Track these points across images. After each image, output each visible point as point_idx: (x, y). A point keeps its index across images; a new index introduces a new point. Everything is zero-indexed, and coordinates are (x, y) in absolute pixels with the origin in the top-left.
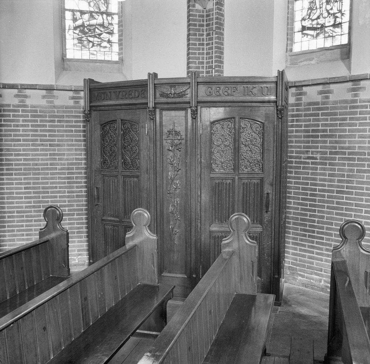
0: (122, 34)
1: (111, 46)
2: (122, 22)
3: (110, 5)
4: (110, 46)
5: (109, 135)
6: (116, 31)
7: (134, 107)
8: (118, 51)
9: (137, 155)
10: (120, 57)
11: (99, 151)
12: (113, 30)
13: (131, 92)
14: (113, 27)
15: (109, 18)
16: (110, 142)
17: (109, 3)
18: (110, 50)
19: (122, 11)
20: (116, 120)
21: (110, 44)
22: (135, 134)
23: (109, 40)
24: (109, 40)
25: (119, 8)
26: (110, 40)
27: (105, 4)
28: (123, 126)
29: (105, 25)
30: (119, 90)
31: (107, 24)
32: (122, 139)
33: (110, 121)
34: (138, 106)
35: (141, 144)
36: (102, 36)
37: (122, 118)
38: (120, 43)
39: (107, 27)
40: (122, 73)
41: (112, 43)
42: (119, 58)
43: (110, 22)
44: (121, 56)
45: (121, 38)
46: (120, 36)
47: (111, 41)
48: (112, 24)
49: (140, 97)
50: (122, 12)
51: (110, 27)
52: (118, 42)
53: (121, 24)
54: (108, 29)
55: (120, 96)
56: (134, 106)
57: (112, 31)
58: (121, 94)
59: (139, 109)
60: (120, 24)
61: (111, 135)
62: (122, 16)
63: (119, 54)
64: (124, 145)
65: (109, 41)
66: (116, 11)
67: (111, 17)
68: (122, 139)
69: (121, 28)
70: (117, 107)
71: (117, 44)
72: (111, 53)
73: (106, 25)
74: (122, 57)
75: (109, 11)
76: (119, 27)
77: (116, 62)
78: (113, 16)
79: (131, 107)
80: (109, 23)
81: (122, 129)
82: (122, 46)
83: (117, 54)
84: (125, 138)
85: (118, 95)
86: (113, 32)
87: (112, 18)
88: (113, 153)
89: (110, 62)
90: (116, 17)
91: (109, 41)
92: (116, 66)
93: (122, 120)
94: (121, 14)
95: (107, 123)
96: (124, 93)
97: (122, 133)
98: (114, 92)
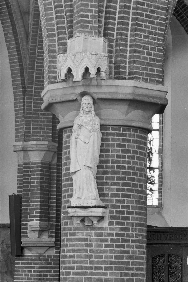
0: (162, 184)
1: (153, 193)
2: (162, 175)
3: (152, 162)
4: (151, 193)
5: (159, 265)
6: (157, 181)
7: (179, 246)
8: (158, 197)
9: (180, 280)
10: (160, 202)
11: (151, 276)
12: (154, 181)
13: (176, 235)
14: (154, 178)
15: (152, 172)
16: (159, 270)
17: (152, 160)
18: (151, 196)
19: (162, 166)
20: (165, 254)
21: (152, 192)
22: (179, 264)
23: (151, 188)
24: (151, 188)
25: (159, 164)
26: (152, 188)
27: (149, 161)
28: (170, 259)
29: (148, 177)
30: (167, 233)
31: (150, 177)
32: (169, 268)
33: (160, 255)
34: (181, 245)
35: (183, 271)
36: (91, 128)
37: (169, 253)
38: (160, 191)
39: (150, 179)
40: (161, 215)
41: (153, 191)
42: (159, 203)
43: (152, 175)
44: (160, 201)
45: (161, 187)
46: (159, 186)
47: (153, 189)
48: (153, 176)
49: (183, 239)
50: (162, 168)
51: (152, 178)
52: (158, 190)
53: (161, 176)
54: (150, 180)
55: (168, 238)
56: (178, 245)
57: (153, 181)
58: (168, 236)
59: (182, 247)
60: (160, 176)
61: (160, 265)
62: (162, 170)
63: (159, 200)
64: (170, 272)
65: (151, 190)
66: (157, 167)
67: (153, 171)
68: (169, 268)
69: (161, 180)
70: (166, 245)
71: (157, 192)
72: (152, 199)
73: (149, 177)
74: (162, 202)
75: (151, 166)
76: (159, 178)
77: (157, 207)
78: (154, 170)
79: (176, 245)
80: (151, 176)
81: (169, 261)
82: (162, 193)
83: (157, 199)
84: (171, 267)
85: (166, 236)
86: (154, 182)
87: (154, 171)
88: (162, 278)
89: (151, 207)
90: (157, 171)
91: (151, 190)
92: (156, 209)
93: (169, 254)
94: (161, 169)
95: (157, 257)
96: (171, 236)
97: (169, 263)
98: (163, 235)
